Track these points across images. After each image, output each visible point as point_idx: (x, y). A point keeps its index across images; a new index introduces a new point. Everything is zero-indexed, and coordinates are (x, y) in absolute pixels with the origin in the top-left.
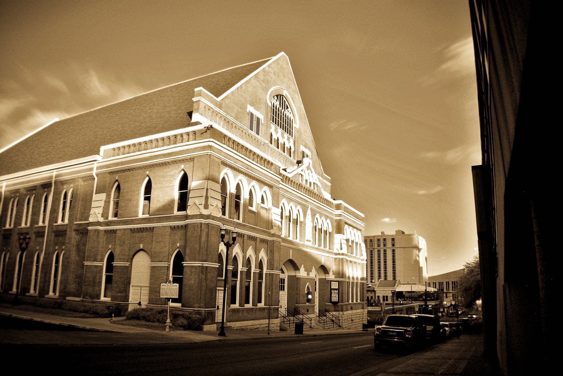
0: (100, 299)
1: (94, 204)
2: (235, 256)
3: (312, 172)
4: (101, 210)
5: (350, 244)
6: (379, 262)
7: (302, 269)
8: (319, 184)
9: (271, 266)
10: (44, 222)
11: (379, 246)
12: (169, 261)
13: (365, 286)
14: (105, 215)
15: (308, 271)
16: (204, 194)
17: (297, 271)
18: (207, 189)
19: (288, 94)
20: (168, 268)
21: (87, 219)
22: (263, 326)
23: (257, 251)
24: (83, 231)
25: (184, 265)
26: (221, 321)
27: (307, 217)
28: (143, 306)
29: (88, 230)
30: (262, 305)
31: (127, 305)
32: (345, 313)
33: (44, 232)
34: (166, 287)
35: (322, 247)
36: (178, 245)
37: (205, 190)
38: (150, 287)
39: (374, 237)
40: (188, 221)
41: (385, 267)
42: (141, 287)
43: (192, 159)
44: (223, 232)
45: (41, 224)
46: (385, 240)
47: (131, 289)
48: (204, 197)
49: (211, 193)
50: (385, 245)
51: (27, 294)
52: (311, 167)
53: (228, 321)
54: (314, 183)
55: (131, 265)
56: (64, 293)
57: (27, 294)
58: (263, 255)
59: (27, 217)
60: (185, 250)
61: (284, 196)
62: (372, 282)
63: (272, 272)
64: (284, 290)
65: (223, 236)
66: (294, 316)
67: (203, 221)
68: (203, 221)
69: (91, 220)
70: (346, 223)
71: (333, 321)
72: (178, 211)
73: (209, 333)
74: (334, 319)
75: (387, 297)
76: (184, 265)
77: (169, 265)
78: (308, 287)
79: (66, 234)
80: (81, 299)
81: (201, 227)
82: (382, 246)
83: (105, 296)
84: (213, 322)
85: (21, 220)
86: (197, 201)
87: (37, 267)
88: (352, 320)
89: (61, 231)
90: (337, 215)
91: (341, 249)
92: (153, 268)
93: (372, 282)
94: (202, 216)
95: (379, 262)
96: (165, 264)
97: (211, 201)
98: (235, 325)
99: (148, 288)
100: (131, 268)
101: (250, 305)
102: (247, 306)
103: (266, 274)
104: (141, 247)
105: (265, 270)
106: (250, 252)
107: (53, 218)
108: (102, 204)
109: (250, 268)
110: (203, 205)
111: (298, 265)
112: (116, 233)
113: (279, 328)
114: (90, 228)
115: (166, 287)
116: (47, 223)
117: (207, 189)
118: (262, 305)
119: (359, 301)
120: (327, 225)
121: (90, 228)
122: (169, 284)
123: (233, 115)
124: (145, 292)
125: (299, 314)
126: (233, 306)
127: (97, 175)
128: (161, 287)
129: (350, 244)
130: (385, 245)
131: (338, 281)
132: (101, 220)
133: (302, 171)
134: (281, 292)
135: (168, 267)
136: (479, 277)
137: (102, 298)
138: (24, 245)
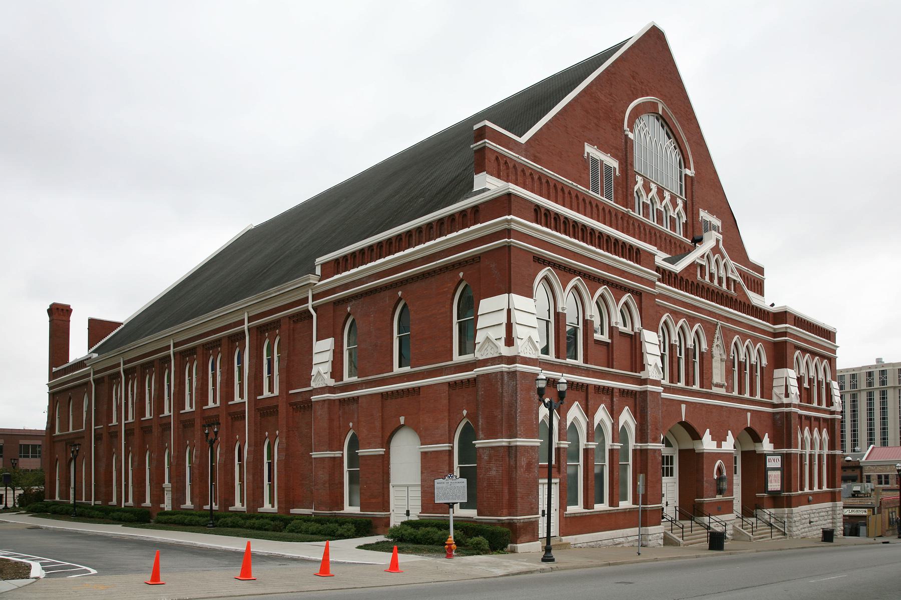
1: (316, 359)
2: (572, 423)
3: (723, 257)
5: (806, 385)
6: (870, 411)
7: (707, 437)
8: (739, 279)
9: (642, 436)
10: (241, 396)
11: (870, 384)
12: (451, 441)
13: (838, 462)
14: (336, 373)
15: (719, 438)
16: (505, 321)
17: (757, 444)
18: (509, 311)
19: (670, 113)
20: (451, 452)
21: (310, 386)
22: (630, 539)
23: (614, 413)
24: (304, 405)
25: (477, 446)
26: (545, 536)
27: (716, 342)
28: (414, 517)
29: (310, 401)
30: (625, 504)
32: (795, 510)
34: (444, 485)
35: (747, 395)
36: (465, 412)
37: (505, 312)
38: (422, 486)
39: (861, 369)
41: (871, 420)
44: (542, 384)
45: (237, 399)
46: (883, 372)
48: (504, 326)
49: (517, 317)
50: (883, 383)
51: (231, 509)
52: (721, 246)
53: (563, 532)
54: (728, 278)
55: (388, 453)
56: (288, 499)
57: (231, 509)
58: (626, 417)
59: (191, 395)
60: (476, 423)
61: (542, 261)
62: (854, 451)
63: (833, 452)
64: (672, 475)
65: (541, 392)
66: (691, 519)
67: (504, 367)
68: (504, 367)
69: (314, 385)
70: (797, 347)
71: (771, 525)
72: (460, 355)
73: (528, 556)
74: (772, 520)
75: (887, 477)
76: (477, 446)
77: (452, 447)
78: (719, 469)
80: (313, 511)
81: (502, 379)
82: (877, 385)
83: (350, 505)
84: (535, 538)
86: (493, 334)
87: (241, 466)
88: (810, 522)
89: (269, 408)
90: (775, 335)
91: (787, 395)
92: (424, 454)
93: (854, 451)
94: (501, 359)
95: (870, 411)
96: (444, 447)
97: (518, 331)
98: (576, 539)
99: (420, 488)
100: (389, 458)
101: (602, 507)
102: (598, 507)
103: (634, 451)
105: (632, 444)
106: (602, 415)
107: (256, 387)
108: (329, 356)
109: (603, 442)
110: (503, 340)
111: (698, 430)
112: (358, 403)
113: (661, 542)
114: (314, 398)
115: (444, 485)
116: (246, 399)
117: (509, 311)
118: (625, 504)
119: (825, 488)
120: (758, 356)
121: (314, 398)
122: (450, 481)
124: (416, 495)
125: (702, 515)
126: (571, 509)
127: (315, 308)
128: (436, 485)
129: (806, 385)
130: (883, 383)
131: (782, 455)
132: (332, 383)
133: (703, 256)
134: (665, 479)
135: (449, 451)
137: (348, 509)
138: (212, 436)
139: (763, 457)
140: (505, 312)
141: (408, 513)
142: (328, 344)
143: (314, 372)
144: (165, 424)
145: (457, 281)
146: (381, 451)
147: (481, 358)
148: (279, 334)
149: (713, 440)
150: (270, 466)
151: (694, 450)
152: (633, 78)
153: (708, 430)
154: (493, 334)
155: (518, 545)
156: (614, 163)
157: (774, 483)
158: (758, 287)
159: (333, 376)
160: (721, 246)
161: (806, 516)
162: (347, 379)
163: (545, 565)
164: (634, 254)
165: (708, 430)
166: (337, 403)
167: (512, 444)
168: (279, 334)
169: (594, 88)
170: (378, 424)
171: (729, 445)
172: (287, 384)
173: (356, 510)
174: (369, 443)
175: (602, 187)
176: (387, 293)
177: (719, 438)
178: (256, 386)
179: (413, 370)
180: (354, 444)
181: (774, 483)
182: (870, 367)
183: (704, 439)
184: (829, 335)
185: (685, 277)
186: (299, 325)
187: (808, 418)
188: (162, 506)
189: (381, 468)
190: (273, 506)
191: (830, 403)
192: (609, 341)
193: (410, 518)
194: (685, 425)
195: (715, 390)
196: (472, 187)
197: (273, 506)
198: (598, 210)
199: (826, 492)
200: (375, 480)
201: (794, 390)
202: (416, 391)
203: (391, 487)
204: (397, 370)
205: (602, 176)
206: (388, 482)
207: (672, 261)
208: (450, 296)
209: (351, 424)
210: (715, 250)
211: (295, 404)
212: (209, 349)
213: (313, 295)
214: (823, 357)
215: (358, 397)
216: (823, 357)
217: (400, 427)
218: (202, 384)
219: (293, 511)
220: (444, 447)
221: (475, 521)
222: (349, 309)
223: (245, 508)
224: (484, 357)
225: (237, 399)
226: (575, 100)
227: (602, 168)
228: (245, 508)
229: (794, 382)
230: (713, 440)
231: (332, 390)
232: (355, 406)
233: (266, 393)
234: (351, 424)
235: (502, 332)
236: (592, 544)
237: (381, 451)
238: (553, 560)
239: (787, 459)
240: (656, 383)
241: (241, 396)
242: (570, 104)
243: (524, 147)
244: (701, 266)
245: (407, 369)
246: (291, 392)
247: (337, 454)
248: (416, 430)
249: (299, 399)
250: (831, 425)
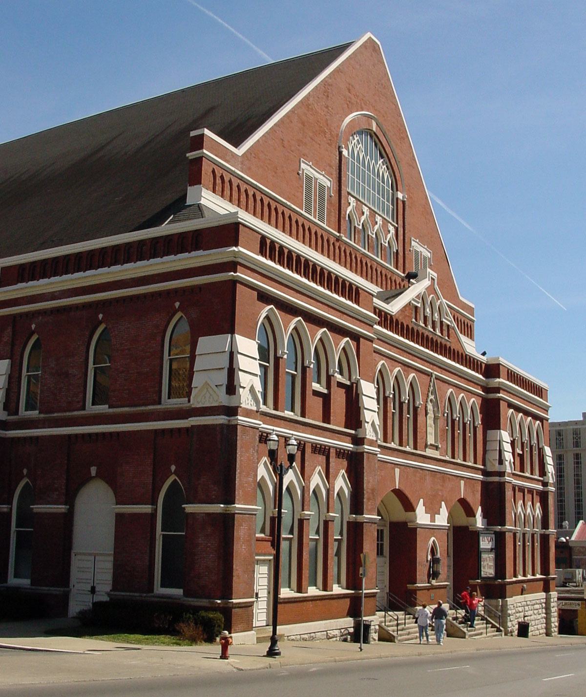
7: (420, 509)
12: (154, 502)
15: (433, 511)
20: (153, 515)
48: (226, 371)
83: (15, 576)
92: (120, 517)
96: (147, 509)
99: (111, 558)
110: (224, 389)
133: (418, 297)
135: (152, 514)
139: (475, 536)
141: (93, 590)
146: (62, 508)
149: (426, 512)
152: (349, 91)
153: (422, 500)
156: (326, 182)
157: (488, 568)
158: (468, 329)
160: (436, 287)
161: (520, 609)
162: (24, 413)
163: (270, 660)
164: (352, 292)
165: (422, 500)
169: (311, 99)
171: (442, 519)
173: (25, 582)
175: (315, 208)
177: (433, 511)
179: (111, 410)
180: (29, 495)
181: (488, 568)
182: (576, 423)
183: (417, 511)
184: (539, 391)
185: (401, 319)
187: (522, 489)
191: (543, 473)
192: (325, 391)
193: (97, 598)
194: (399, 493)
195: (430, 452)
196: (186, 203)
198: (310, 234)
199: (540, 580)
200: (53, 545)
201: (508, 456)
204: (92, 409)
205: (315, 195)
207: (388, 299)
209: (25, 471)
210: (431, 289)
214: (536, 417)
216: (536, 417)
220: (147, 509)
226: (292, 111)
227: (315, 188)
229: (507, 447)
230: (426, 512)
234: (25, 471)
236: (306, 636)
237: (62, 508)
238: (278, 654)
239: (500, 539)
240: (372, 443)
242: (287, 116)
243: (240, 159)
244: (416, 307)
245: (103, 409)
250: (543, 497)
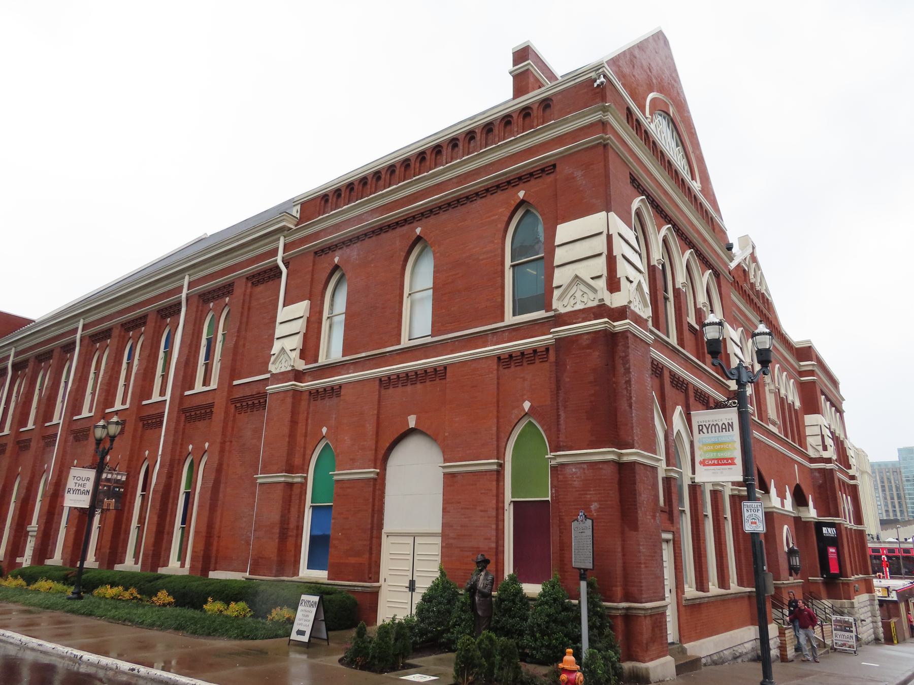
0: (296, 573)
1: (280, 330)
4: (296, 342)
10: (162, 393)
12: (500, 455)
29: (265, 395)
31: (374, 595)
33: (162, 415)
36: (527, 405)
38: (444, 535)
40: (564, 330)
42: (414, 536)
43: (549, 169)
45: (156, 398)
47: (387, 546)
56: (206, 559)
59: (126, 386)
72: (514, 315)
79: (211, 412)
80: (247, 575)
83: (310, 566)
85: (114, 396)
86: (586, 270)
89: (199, 407)
92: (450, 478)
94: (601, 310)
96: (489, 464)
99: (438, 540)
104: (412, 422)
112: (338, 395)
116: (168, 397)
121: (271, 388)
123: (297, 478)
127: (286, 264)
132: (301, 365)
136: (759, 652)
140: (604, 238)
142: (301, 308)
143: (276, 349)
144: (49, 436)
145: (514, 204)
146: (369, 472)
147: (563, 310)
148: (214, 309)
150: (188, 496)
151: (765, 534)
154: (586, 270)
155: (650, 665)
159: (303, 355)
166: (306, 396)
167: (625, 459)
168: (214, 309)
170: (370, 428)
172: (232, 370)
174: (353, 460)
176: (500, 196)
178: (184, 377)
186: (261, 288)
188: (18, 560)
189: (366, 506)
190: (183, 566)
197: (183, 566)
202: (439, 373)
203: (384, 536)
206: (380, 526)
208: (501, 226)
209: (324, 430)
211: (240, 400)
212: (128, 330)
213: (285, 245)
215: (340, 386)
217: (410, 433)
218: (111, 377)
219: (213, 575)
221: (779, 552)
222: (336, 260)
223: (138, 568)
224: (569, 309)
225: (156, 398)
228: (138, 568)
231: (298, 375)
232: (335, 400)
233: (199, 387)
234: (324, 430)
235: (600, 266)
241: (162, 393)
246: (235, 383)
247: (297, 478)
248: (432, 436)
249: (248, 392)
